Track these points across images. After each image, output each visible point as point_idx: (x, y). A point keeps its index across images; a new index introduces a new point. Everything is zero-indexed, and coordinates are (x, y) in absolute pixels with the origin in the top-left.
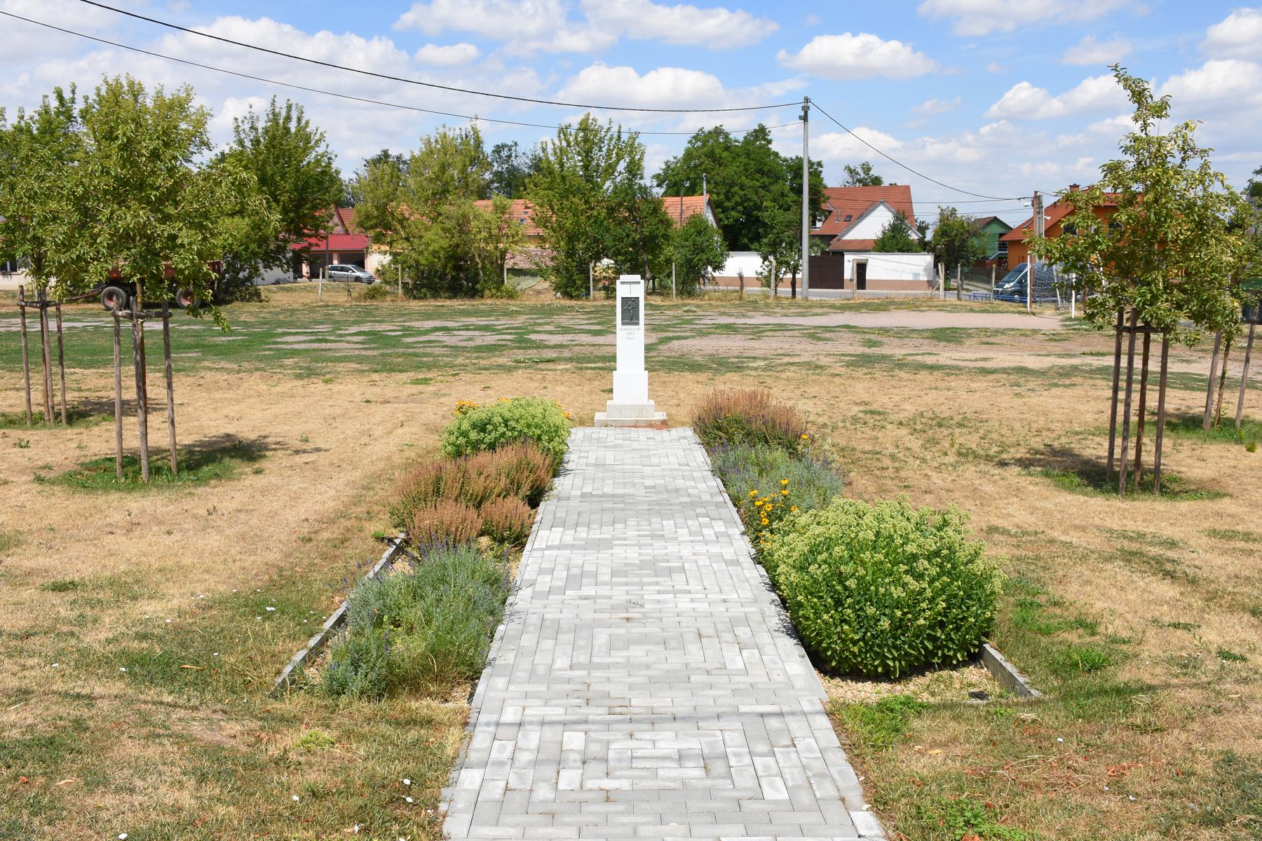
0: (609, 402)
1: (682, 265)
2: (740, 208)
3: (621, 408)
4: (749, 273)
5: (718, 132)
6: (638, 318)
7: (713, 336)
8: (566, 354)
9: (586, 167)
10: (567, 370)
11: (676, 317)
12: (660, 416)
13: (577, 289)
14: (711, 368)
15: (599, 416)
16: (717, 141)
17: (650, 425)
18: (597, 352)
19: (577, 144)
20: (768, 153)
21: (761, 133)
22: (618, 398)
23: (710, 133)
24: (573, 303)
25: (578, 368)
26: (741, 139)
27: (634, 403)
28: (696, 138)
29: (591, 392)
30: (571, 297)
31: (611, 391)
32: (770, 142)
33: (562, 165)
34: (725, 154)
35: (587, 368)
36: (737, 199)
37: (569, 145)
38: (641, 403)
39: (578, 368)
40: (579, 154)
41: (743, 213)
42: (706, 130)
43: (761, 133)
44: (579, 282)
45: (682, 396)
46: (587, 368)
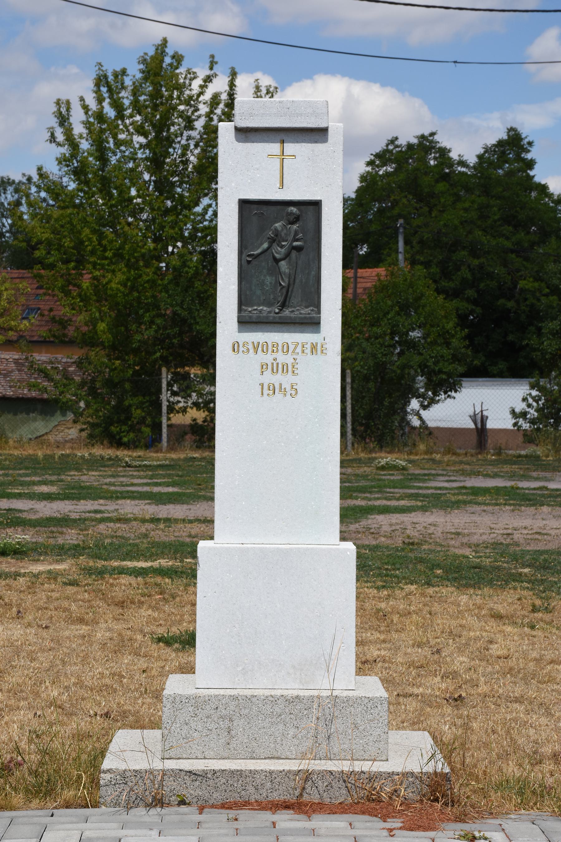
0: (175, 685)
1: (366, 379)
2: (470, 293)
3: (228, 714)
4: (500, 420)
5: (426, 144)
6: (314, 298)
7: (470, 508)
8: (71, 536)
9: (156, 163)
10: (52, 576)
11: (365, 477)
12: (410, 753)
13: (132, 428)
14: (518, 578)
15: (128, 752)
16: (425, 162)
17: (369, 798)
18: (160, 535)
19: (137, 107)
20: (529, 184)
21: (513, 146)
22: (215, 670)
23: (410, 146)
24: (120, 453)
25: (88, 571)
26: (472, 160)
27: (291, 688)
28: (382, 157)
29: (121, 645)
30: (119, 444)
31: (189, 641)
32: (530, 164)
33: (103, 158)
34: (441, 186)
35: (122, 571)
36: (465, 273)
37: (120, 116)
38: (321, 686)
39: (88, 571)
40: (140, 130)
41: (475, 302)
42: (402, 141)
43: (513, 146)
44: (137, 413)
45: (460, 662)
46: (122, 571)
